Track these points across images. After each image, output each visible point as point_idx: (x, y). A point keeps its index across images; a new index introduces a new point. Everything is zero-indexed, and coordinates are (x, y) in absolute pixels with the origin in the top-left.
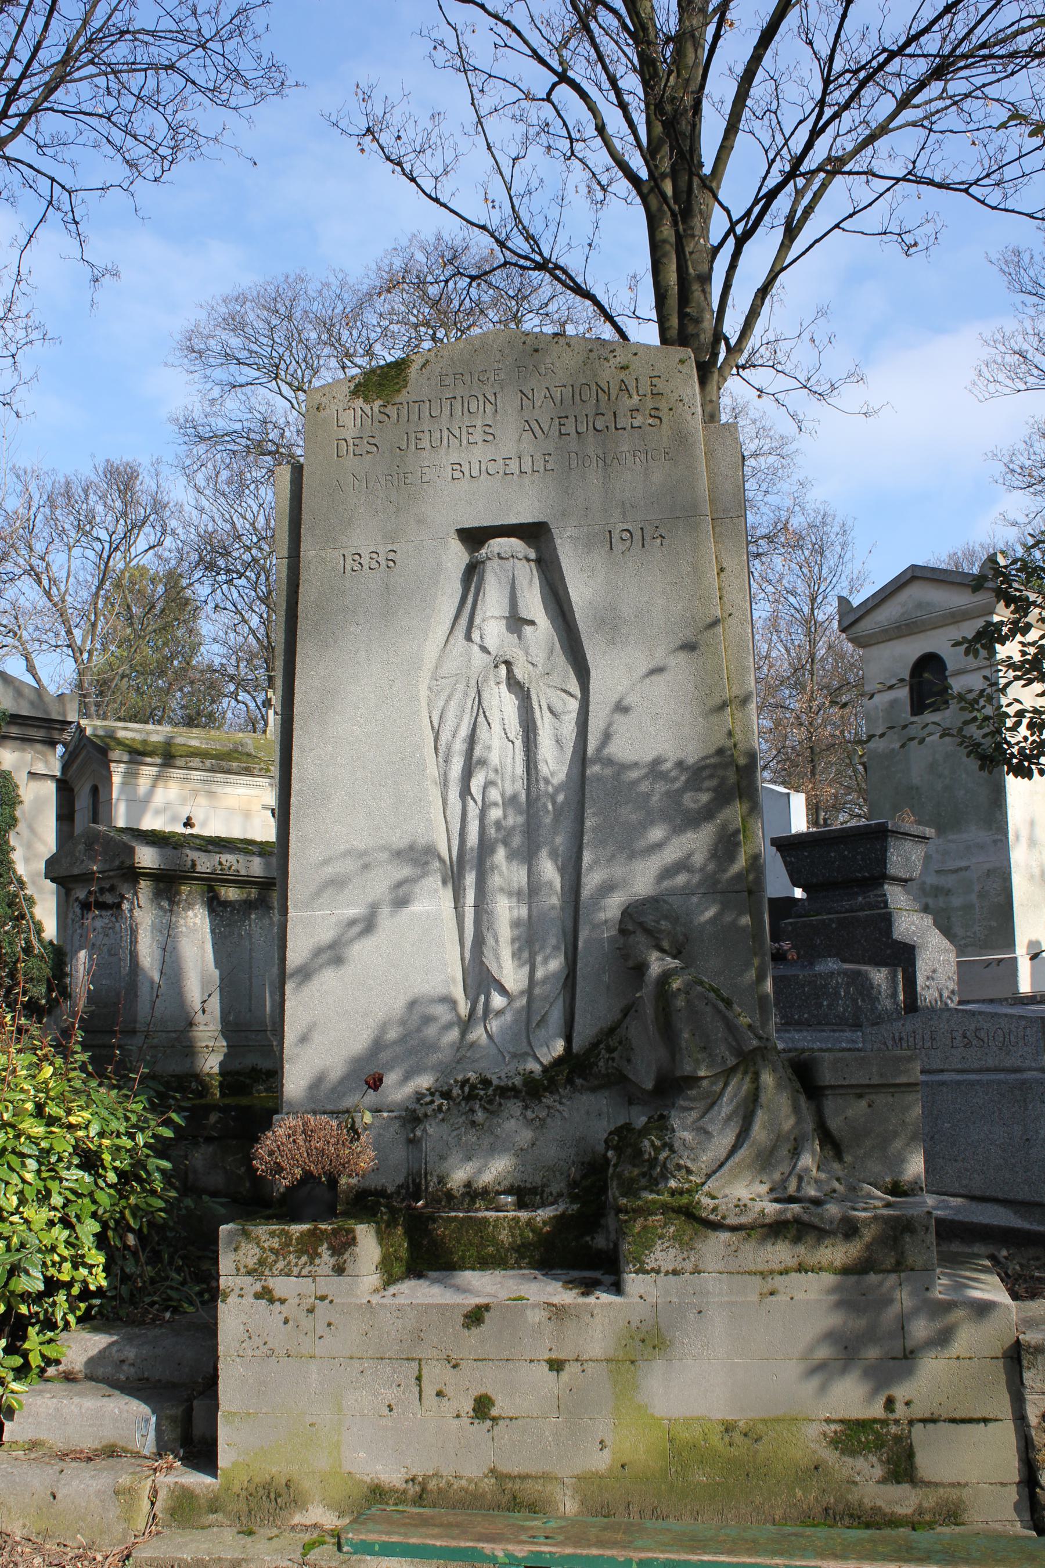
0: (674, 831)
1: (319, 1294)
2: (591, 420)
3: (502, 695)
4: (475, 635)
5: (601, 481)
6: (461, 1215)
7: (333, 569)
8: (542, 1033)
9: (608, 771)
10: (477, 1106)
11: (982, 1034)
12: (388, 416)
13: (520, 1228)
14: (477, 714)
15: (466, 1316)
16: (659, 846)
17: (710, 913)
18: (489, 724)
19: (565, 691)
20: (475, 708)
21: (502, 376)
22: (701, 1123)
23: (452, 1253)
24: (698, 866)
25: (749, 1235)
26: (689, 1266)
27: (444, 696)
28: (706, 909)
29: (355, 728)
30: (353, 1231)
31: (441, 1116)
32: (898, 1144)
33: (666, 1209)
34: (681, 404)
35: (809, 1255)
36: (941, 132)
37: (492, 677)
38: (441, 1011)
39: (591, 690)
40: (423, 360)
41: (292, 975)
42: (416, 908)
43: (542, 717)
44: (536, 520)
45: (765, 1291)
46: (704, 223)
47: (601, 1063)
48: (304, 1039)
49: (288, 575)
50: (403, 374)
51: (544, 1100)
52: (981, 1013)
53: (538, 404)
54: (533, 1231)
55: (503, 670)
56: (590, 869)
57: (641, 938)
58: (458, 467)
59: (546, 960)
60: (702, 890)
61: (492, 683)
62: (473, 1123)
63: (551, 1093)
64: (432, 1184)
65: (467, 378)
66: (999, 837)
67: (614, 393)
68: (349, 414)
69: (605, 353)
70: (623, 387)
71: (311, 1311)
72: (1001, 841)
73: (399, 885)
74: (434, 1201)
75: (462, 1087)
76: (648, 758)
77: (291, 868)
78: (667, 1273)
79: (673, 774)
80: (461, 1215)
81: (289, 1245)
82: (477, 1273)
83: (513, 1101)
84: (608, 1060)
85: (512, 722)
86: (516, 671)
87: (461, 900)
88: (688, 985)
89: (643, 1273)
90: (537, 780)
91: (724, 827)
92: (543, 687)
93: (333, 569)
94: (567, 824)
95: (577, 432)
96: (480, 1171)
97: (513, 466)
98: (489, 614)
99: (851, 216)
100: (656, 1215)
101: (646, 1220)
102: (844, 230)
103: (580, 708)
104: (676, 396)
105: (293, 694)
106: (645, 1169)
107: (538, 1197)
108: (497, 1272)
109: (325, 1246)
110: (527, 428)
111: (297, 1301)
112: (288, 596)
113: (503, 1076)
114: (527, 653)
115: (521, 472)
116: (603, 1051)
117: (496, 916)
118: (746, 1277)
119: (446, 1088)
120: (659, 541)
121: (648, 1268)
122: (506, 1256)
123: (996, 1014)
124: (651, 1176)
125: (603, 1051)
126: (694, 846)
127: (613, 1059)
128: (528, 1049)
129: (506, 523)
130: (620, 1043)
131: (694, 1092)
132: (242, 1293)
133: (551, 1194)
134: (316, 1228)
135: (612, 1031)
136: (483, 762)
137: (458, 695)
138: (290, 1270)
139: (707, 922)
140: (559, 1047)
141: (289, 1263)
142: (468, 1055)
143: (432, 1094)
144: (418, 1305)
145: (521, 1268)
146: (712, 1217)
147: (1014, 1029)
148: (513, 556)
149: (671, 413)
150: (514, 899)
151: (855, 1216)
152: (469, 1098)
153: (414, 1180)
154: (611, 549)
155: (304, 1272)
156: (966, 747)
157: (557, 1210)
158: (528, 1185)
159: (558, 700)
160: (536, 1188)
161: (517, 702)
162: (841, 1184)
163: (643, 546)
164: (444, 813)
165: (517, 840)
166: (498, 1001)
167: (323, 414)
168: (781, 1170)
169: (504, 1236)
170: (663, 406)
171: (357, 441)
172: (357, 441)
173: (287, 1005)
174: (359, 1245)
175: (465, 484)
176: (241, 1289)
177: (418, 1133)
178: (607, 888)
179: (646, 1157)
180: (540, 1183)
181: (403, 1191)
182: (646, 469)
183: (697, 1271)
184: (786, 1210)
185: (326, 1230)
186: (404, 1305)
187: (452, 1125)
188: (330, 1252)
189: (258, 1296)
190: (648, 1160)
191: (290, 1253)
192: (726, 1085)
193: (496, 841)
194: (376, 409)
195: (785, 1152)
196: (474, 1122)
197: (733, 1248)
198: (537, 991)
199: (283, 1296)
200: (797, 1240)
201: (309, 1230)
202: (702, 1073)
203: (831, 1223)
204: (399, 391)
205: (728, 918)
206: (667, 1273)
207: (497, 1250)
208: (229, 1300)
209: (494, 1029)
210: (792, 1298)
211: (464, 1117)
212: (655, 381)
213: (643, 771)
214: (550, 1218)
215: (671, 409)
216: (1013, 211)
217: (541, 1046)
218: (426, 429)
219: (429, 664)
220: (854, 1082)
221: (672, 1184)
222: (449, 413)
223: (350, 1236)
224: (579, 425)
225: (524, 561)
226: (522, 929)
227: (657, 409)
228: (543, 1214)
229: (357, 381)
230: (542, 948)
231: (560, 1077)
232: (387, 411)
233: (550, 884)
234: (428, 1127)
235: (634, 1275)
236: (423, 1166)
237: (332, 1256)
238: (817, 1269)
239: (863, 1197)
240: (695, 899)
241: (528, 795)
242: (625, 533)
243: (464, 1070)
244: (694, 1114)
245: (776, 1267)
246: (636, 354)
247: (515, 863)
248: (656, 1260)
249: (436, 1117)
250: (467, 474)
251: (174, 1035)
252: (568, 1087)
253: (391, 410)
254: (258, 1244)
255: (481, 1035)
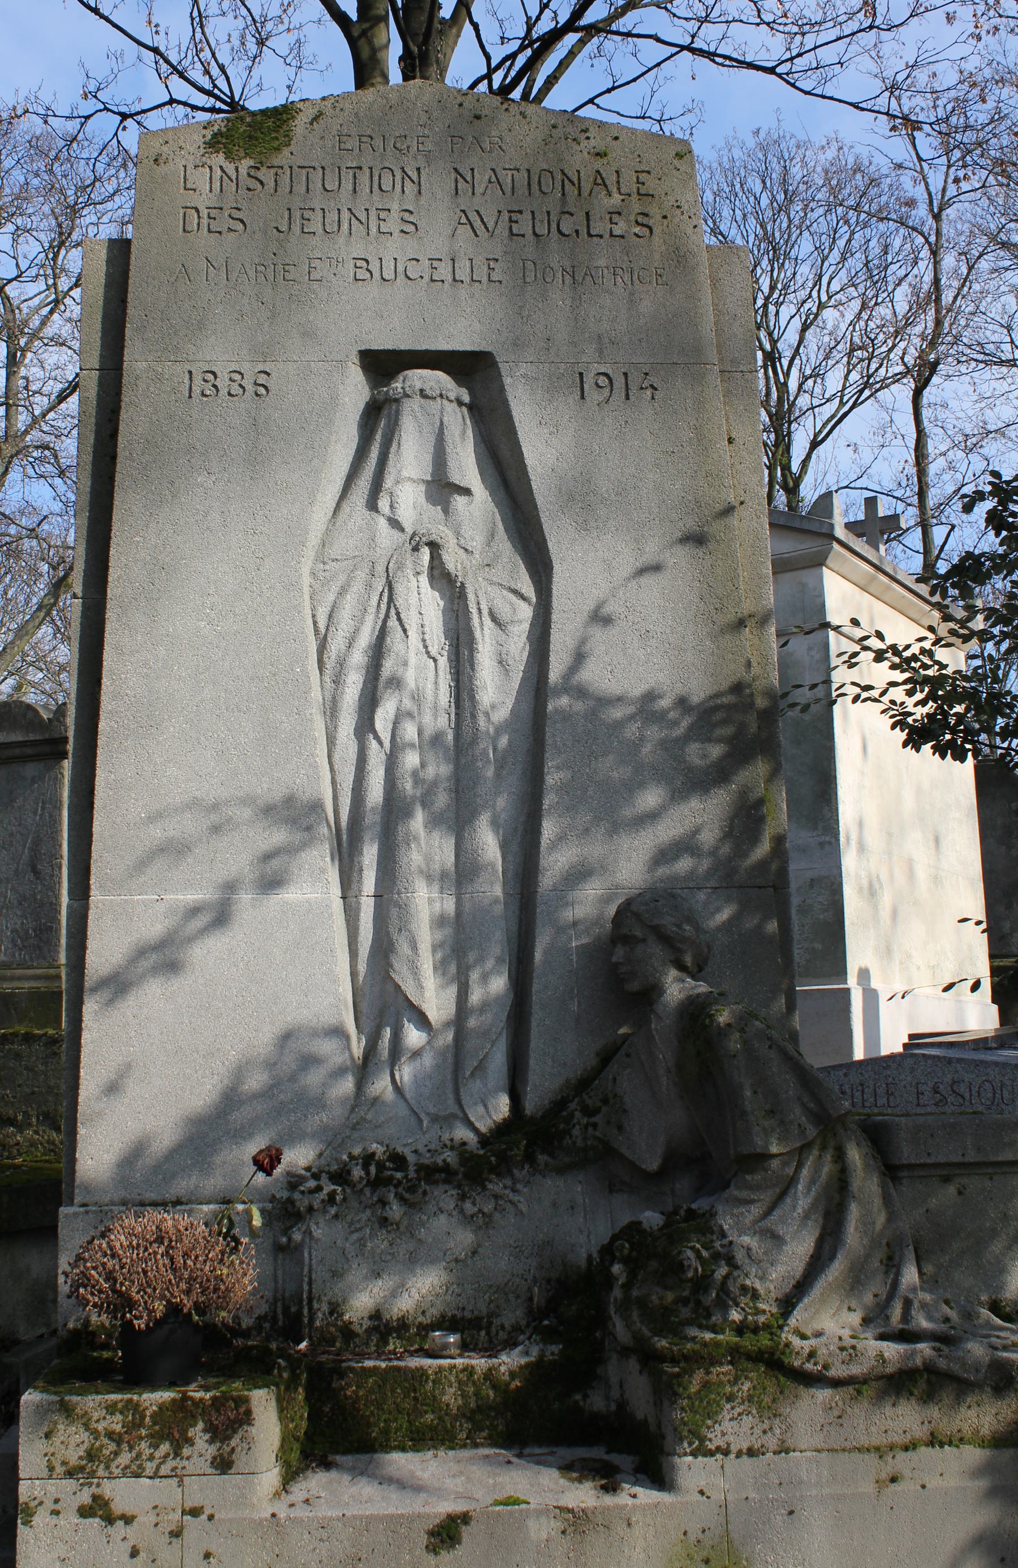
0: (672, 798)
1: (189, 1505)
2: (554, 218)
3: (422, 591)
4: (383, 504)
5: (568, 302)
6: (383, 1365)
7: (174, 391)
8: (476, 1086)
9: (579, 706)
10: (392, 1195)
11: (963, 1089)
12: (261, 183)
13: (474, 1383)
14: (387, 616)
15: (431, 1533)
16: (652, 817)
17: (724, 915)
18: (405, 631)
19: (515, 592)
20: (384, 607)
21: (429, 146)
22: (767, 1223)
23: (369, 1425)
24: (706, 848)
25: (859, 1392)
26: (772, 1442)
27: (335, 588)
28: (718, 910)
29: (203, 624)
30: (247, 1400)
31: (333, 1211)
32: (996, 1247)
33: (736, 1355)
34: (678, 212)
35: (945, 1420)
36: (686, 19)
37: (409, 564)
38: (327, 1047)
39: (554, 592)
40: (315, 111)
41: (94, 990)
42: (291, 895)
43: (482, 624)
44: (477, 349)
45: (884, 1476)
46: (441, 75)
47: (576, 1132)
48: (113, 1088)
49: (98, 395)
50: (285, 127)
51: (490, 1186)
52: (959, 1060)
53: (479, 190)
54: (494, 1387)
55: (425, 553)
56: (553, 846)
57: (655, 950)
58: (364, 264)
59: (485, 978)
60: (713, 883)
61: (410, 572)
62: (384, 1221)
63: (499, 1175)
64: (320, 1315)
65: (378, 142)
66: (827, 839)
67: (586, 187)
68: (203, 175)
69: (573, 131)
70: (600, 180)
71: (176, 1534)
72: (830, 843)
73: (267, 857)
74: (322, 1341)
75: (366, 1166)
76: (637, 690)
77: (96, 828)
78: (739, 1454)
79: (672, 715)
80: (383, 1365)
81: (141, 1425)
82: (410, 1455)
83: (442, 1187)
84: (586, 1127)
85: (435, 631)
86: (445, 557)
87: (354, 886)
88: (741, 1018)
89: (705, 1455)
90: (474, 716)
91: (743, 793)
92: (484, 584)
93: (174, 391)
94: (514, 781)
95: (535, 234)
96: (394, 1294)
97: (444, 271)
98: (405, 474)
99: (609, 91)
100: (721, 1364)
101: (708, 1373)
102: (598, 106)
103: (535, 617)
104: (671, 200)
105: (106, 568)
106: (686, 1293)
107: (483, 1333)
108: (441, 1453)
109: (200, 1425)
110: (464, 220)
111: (152, 1518)
112: (97, 424)
113: (422, 1149)
114: (458, 535)
115: (454, 280)
116: (578, 1114)
117: (413, 911)
118: (856, 1456)
119: (335, 1167)
120: (649, 392)
121: (711, 1446)
122: (453, 1427)
123: (982, 1062)
124: (698, 1303)
125: (578, 1114)
126: (699, 821)
127: (595, 1126)
128: (454, 1109)
129: (433, 348)
130: (605, 1101)
131: (758, 1177)
132: (57, 1507)
133: (503, 1327)
134: (185, 1398)
135: (583, 1084)
136: (396, 683)
137: (357, 587)
138: (140, 1466)
139: (719, 929)
140: (502, 1106)
141: (139, 1455)
142: (369, 1117)
143: (316, 1176)
144: (354, 1517)
145: (476, 1446)
146: (809, 1366)
147: (1009, 1083)
148: (441, 396)
149: (665, 222)
150: (436, 887)
151: (1008, 1360)
152: (377, 1183)
153: (286, 1309)
154: (583, 397)
155: (165, 1470)
156: (892, 717)
157: (527, 1353)
158: (468, 1315)
159: (504, 603)
160: (479, 1319)
161: (442, 603)
162: (951, 1308)
163: (627, 397)
164: (330, 757)
165: (442, 800)
166: (414, 1036)
167: (162, 169)
168: (874, 1290)
169: (450, 1397)
170: (654, 210)
171: (214, 213)
172: (214, 213)
173: (86, 1037)
174: (256, 1423)
175: (373, 289)
176: (57, 1501)
177: (297, 1237)
178: (579, 875)
179: (690, 1274)
180: (485, 1311)
181: (267, 1325)
182: (632, 294)
183: (784, 1449)
184: (914, 1352)
185: (201, 1399)
186: (331, 1519)
187: (351, 1223)
188: (207, 1436)
189: (85, 1512)
190: (691, 1280)
191: (141, 1438)
192: (800, 1166)
193: (414, 798)
194: (243, 171)
195: (877, 1264)
196: (386, 1219)
197: (836, 1413)
198: (472, 1023)
199: (129, 1511)
200: (928, 1397)
201: (174, 1400)
202: (774, 1149)
203: (977, 1371)
204: (278, 149)
205: (750, 923)
206: (739, 1454)
207: (440, 1418)
208: (37, 1520)
209: (406, 1078)
210: (923, 1487)
211: (368, 1212)
212: (643, 177)
213: (631, 710)
214: (521, 1367)
215: (665, 217)
216: (831, 98)
217: (476, 1104)
218: (318, 207)
219: (314, 540)
220: (942, 1159)
221: (735, 1316)
222: (351, 188)
223: (242, 1410)
224: (538, 224)
225: (455, 404)
226: (448, 931)
227: (646, 215)
228: (509, 1361)
229: (216, 128)
230: (481, 960)
231: (515, 1151)
232: (260, 175)
233: (493, 865)
234: (313, 1227)
235: (690, 1458)
236: (306, 1287)
237: (211, 1441)
238: (956, 1441)
239: (981, 1326)
240: (702, 896)
241: (457, 736)
242: (602, 377)
243: (363, 1139)
244: (756, 1210)
245: (898, 1439)
246: (616, 138)
247: (436, 835)
248: (723, 1434)
249: (325, 1211)
250: (377, 274)
251: (862, 1118)
252: (527, 1167)
253: (264, 174)
254: (86, 1426)
255: (386, 1087)
